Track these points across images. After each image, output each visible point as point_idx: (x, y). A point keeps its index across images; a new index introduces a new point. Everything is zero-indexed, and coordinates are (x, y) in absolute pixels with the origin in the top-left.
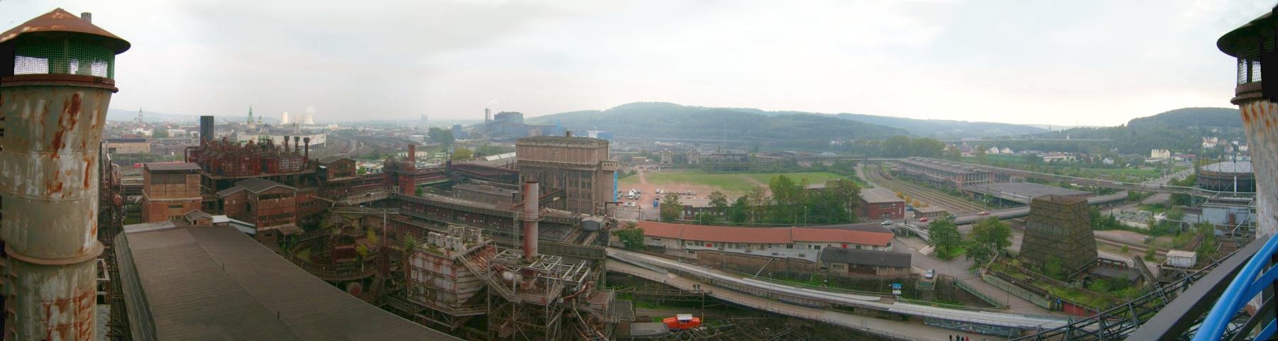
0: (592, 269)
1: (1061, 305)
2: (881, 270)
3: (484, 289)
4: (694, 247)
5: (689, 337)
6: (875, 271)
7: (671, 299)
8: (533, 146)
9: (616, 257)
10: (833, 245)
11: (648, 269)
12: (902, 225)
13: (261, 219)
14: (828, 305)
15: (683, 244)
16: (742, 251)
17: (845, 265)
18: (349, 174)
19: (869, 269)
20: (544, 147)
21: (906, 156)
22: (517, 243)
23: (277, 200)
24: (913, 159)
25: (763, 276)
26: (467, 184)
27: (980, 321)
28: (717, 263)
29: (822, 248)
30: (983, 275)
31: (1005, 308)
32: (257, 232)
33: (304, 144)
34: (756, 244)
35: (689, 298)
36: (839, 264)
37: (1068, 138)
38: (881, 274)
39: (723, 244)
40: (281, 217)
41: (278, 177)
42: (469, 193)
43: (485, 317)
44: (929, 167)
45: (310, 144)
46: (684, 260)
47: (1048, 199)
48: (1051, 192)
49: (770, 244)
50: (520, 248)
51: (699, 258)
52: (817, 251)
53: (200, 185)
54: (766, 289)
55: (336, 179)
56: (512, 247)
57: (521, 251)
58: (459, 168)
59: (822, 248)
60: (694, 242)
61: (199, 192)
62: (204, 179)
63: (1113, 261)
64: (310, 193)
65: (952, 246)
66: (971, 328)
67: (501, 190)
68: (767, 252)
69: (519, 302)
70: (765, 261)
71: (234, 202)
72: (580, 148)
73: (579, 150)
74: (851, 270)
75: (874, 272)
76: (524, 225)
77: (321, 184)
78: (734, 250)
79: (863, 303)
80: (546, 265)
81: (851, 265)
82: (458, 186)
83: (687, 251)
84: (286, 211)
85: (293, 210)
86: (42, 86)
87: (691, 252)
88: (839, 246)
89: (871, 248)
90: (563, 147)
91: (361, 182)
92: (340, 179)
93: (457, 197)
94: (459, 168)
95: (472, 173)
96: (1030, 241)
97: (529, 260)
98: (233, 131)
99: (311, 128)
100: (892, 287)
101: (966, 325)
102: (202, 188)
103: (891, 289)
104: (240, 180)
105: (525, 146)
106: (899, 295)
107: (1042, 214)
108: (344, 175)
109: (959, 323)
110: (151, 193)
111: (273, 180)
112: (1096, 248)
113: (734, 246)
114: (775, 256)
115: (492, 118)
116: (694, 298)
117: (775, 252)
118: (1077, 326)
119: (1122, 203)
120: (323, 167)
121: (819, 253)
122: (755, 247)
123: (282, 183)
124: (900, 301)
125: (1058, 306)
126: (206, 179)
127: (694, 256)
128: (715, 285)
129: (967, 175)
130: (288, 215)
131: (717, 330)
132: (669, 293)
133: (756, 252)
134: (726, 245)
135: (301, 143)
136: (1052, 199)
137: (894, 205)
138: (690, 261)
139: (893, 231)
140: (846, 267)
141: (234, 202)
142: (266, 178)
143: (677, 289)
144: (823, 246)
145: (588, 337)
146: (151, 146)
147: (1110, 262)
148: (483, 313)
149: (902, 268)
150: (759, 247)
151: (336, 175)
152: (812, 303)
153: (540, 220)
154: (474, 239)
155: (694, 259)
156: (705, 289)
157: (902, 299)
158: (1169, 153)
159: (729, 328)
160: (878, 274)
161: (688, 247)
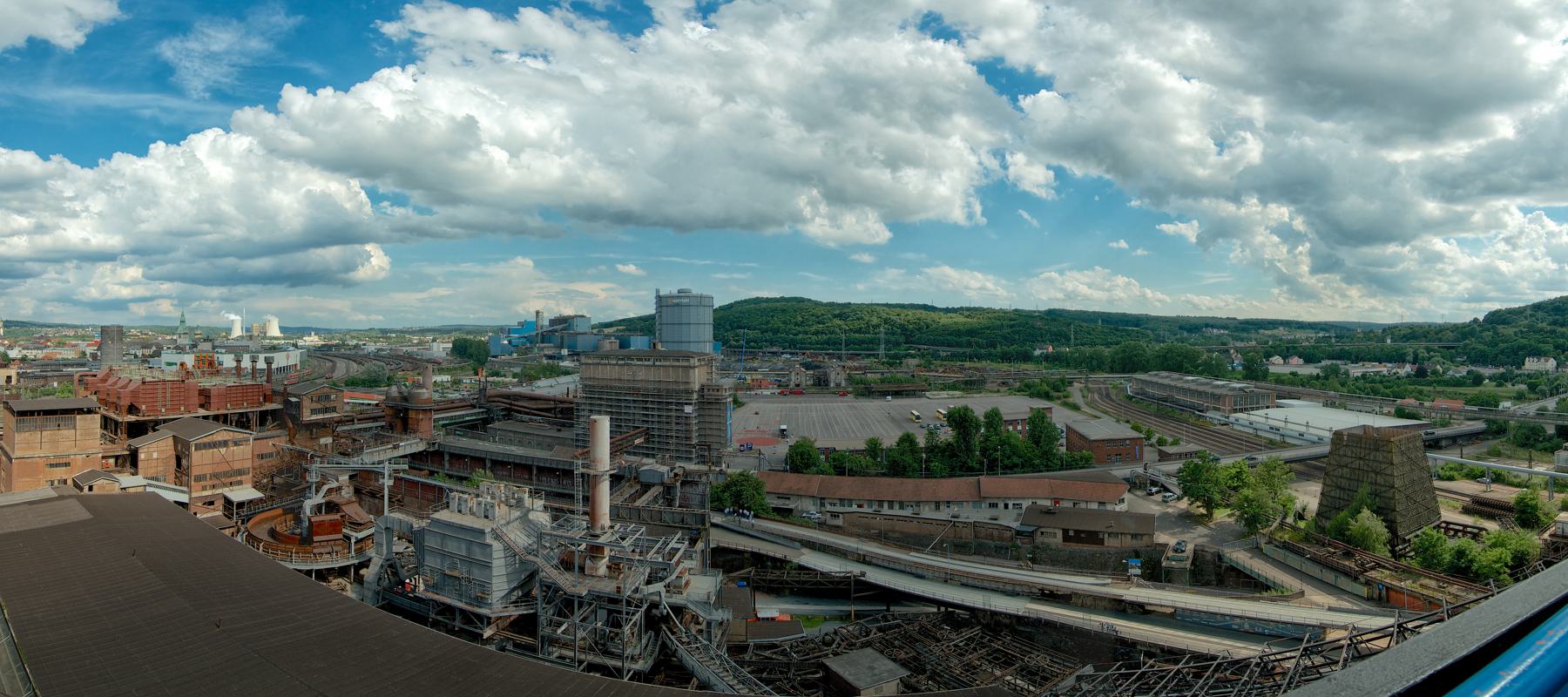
0: (690, 544)
1: (1384, 592)
2: (1111, 539)
3: (532, 576)
4: (838, 509)
5: (834, 641)
6: (1103, 539)
7: (807, 586)
8: (606, 364)
9: (725, 525)
10: (1040, 502)
11: (772, 542)
12: (1140, 470)
13: (199, 478)
14: (1034, 590)
15: (823, 505)
16: (908, 512)
17: (1057, 531)
18: (334, 410)
19: (1093, 537)
20: (620, 365)
21: (1145, 370)
22: (580, 507)
23: (223, 450)
24: (1156, 375)
25: (939, 550)
26: (509, 421)
27: (1260, 616)
28: (872, 531)
29: (1024, 507)
30: (1263, 546)
31: (1284, 597)
32: (190, 499)
33: (265, 366)
34: (927, 502)
35: (832, 583)
36: (1048, 530)
37: (1389, 341)
38: (1111, 545)
39: (881, 503)
40: (232, 476)
41: (226, 415)
42: (511, 434)
43: (534, 617)
44: (1179, 385)
45: (274, 366)
46: (821, 526)
47: (1360, 432)
48: (1362, 423)
49: (948, 502)
50: (585, 513)
51: (846, 525)
52: (1016, 511)
53: (99, 431)
54: (944, 568)
55: (314, 417)
56: (572, 512)
57: (587, 517)
58: (496, 399)
59: (1024, 507)
60: (838, 502)
61: (99, 442)
62: (106, 422)
63: (1466, 526)
64: (276, 441)
65: (1377, 545)
66: (1247, 626)
67: (559, 430)
68: (944, 514)
69: (584, 593)
70: (942, 528)
71: (155, 455)
72: (673, 366)
73: (671, 368)
74: (1066, 538)
75: (1101, 542)
76: (590, 481)
77: (291, 425)
78: (897, 511)
79: (1086, 587)
80: (623, 539)
81: (1065, 532)
82: (497, 425)
83: (829, 514)
84: (237, 466)
85: (248, 464)
86: (767, 541)
87: (835, 515)
88: (1048, 503)
89: (1094, 506)
90: (647, 366)
91: (353, 420)
92: (320, 416)
93: (494, 441)
94: (496, 399)
95: (517, 406)
96: (1333, 494)
97: (598, 532)
98: (154, 348)
99: (275, 342)
100: (1127, 564)
101: (1238, 620)
102: (103, 436)
103: (1126, 568)
104: (165, 421)
105: (593, 364)
106: (1137, 576)
107: (1349, 454)
108: (326, 410)
109: (1228, 618)
110: (16, 446)
111: (218, 421)
112: (1437, 508)
113: (897, 506)
114: (956, 520)
115: (546, 323)
116: (839, 583)
117: (956, 514)
118: (1410, 625)
119: (1477, 439)
120: (293, 399)
121: (1019, 515)
122: (927, 508)
123: (231, 424)
124: (1139, 586)
125: (1380, 594)
126: (109, 421)
127: (839, 522)
128: (869, 564)
129: (1235, 396)
130: (240, 472)
131: (874, 630)
132: (804, 578)
133: (927, 512)
134: (897, 506)
135: (261, 365)
136: (1365, 433)
137: (1128, 442)
138: (836, 529)
139: (1127, 480)
140: (1060, 534)
141: (155, 455)
142: (205, 418)
143: (814, 570)
144: (1026, 504)
145: (682, 643)
146: (18, 373)
147: (1461, 528)
148: (532, 611)
149: (1142, 535)
150: (933, 506)
151: (313, 412)
152: (1009, 588)
153: (612, 472)
154: (518, 502)
155: (838, 527)
156: (855, 569)
157: (1142, 581)
158: (1555, 363)
159: (890, 627)
160: (1106, 544)
161: (829, 508)
